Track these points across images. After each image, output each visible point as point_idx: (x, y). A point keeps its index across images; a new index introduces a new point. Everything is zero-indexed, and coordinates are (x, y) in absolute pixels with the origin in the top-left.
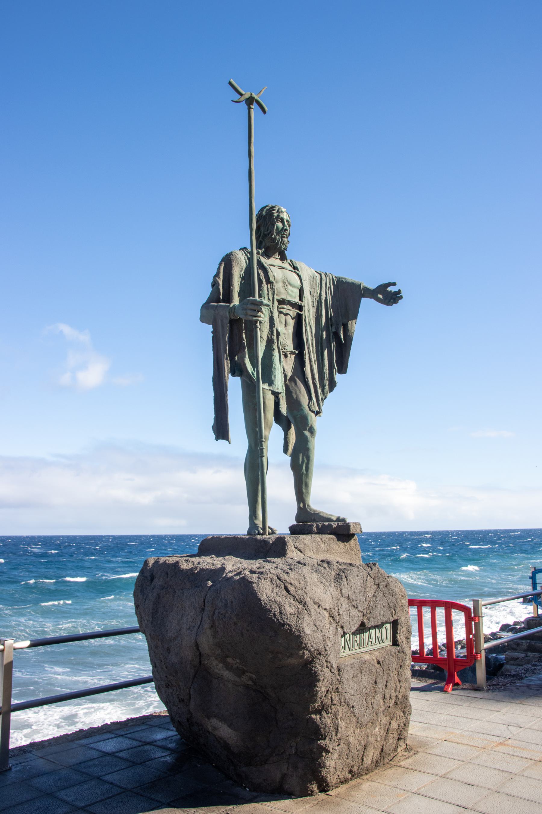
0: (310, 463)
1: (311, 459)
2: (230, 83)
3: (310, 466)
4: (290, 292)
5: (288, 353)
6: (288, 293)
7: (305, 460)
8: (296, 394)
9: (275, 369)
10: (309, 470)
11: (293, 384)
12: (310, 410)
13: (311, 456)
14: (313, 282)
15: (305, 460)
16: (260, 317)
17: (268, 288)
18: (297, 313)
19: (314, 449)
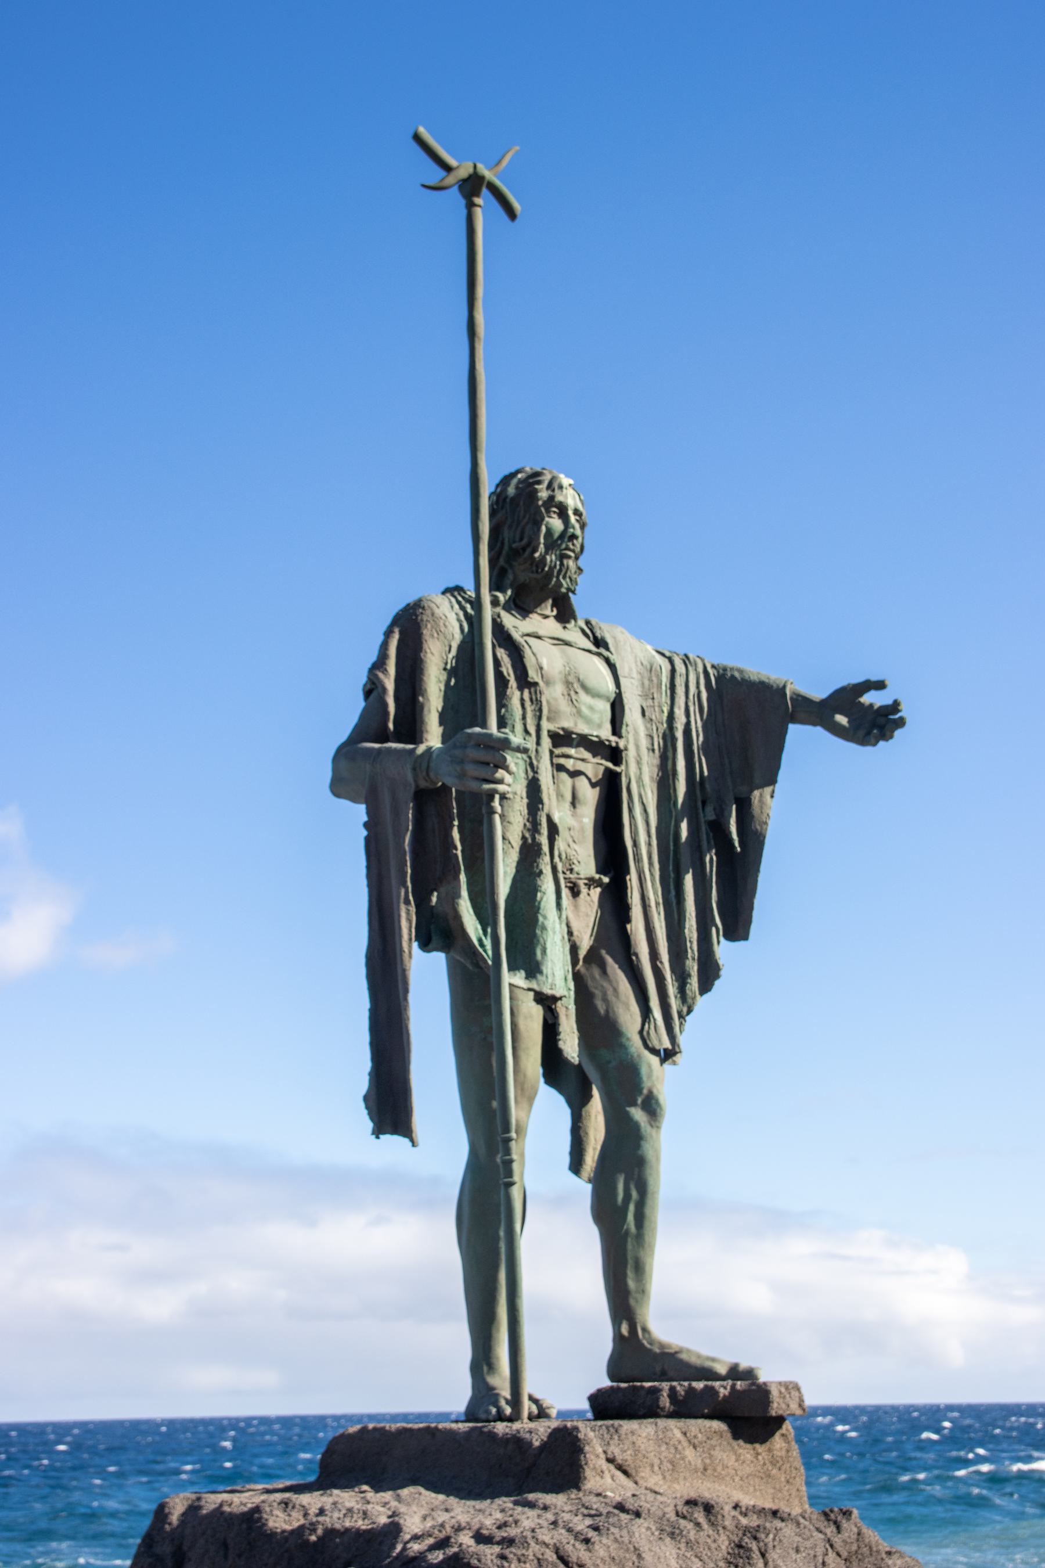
0: (649, 1202)
1: (651, 1188)
2: (417, 138)
3: (647, 1211)
4: (585, 710)
5: (581, 883)
6: (579, 712)
7: (634, 1194)
8: (605, 1000)
9: (544, 928)
10: (647, 1224)
11: (596, 972)
12: (646, 1046)
13: (651, 1181)
14: (651, 680)
15: (634, 1194)
16: (501, 782)
17: (522, 700)
18: (607, 769)
19: (658, 1159)
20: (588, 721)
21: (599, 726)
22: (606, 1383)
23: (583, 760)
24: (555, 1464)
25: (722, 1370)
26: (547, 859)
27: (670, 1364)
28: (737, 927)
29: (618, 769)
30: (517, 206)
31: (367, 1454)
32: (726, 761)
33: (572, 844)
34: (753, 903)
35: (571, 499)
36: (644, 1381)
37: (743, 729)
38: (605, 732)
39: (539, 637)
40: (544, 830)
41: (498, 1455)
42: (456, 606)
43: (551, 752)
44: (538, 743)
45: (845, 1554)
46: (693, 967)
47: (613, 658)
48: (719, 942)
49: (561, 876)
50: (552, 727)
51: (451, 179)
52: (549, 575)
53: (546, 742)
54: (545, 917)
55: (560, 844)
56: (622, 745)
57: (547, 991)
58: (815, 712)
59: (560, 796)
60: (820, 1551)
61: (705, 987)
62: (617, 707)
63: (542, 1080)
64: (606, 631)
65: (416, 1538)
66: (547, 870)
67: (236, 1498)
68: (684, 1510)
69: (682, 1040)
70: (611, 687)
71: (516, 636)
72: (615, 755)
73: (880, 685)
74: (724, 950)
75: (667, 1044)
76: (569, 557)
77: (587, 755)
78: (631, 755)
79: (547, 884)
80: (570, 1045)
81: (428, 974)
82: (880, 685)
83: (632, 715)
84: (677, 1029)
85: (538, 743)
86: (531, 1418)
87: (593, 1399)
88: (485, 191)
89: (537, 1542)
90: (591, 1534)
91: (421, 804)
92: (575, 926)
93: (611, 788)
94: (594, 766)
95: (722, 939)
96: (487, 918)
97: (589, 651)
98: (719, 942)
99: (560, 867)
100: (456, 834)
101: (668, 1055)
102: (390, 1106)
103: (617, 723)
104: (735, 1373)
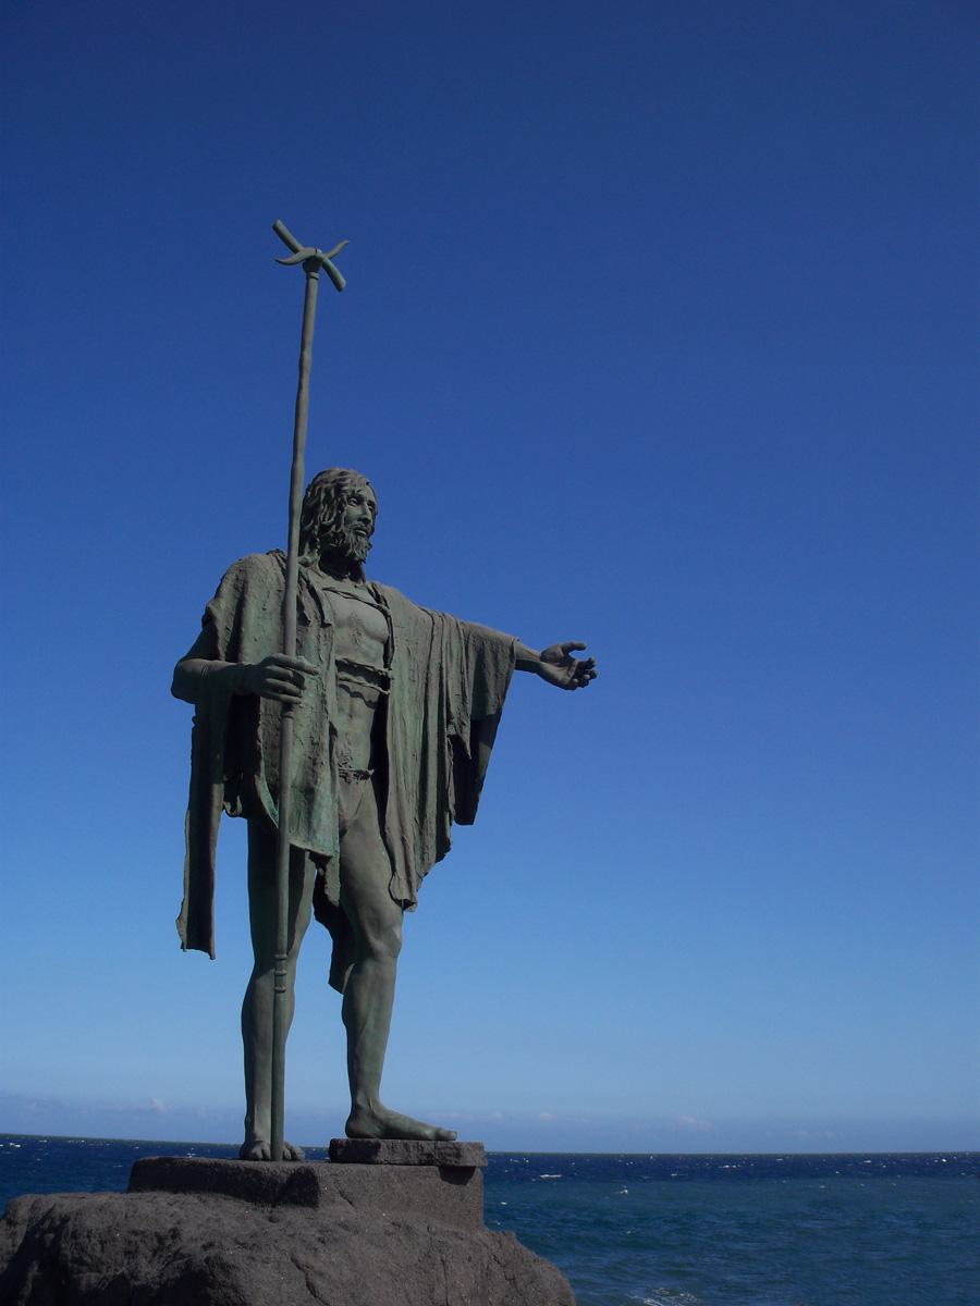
2: (276, 229)
20: (366, 655)
21: (375, 660)
22: (343, 1136)
23: (360, 684)
24: (300, 1189)
25: (428, 1132)
26: (327, 754)
27: (392, 1131)
28: (466, 815)
29: (386, 693)
30: (343, 281)
31: (161, 1169)
32: (323, 648)
33: (348, 746)
34: (476, 800)
35: (367, 494)
36: (367, 1139)
37: (489, 670)
38: (379, 666)
39: (335, 592)
40: (327, 733)
41: (254, 1176)
42: (276, 563)
43: (337, 677)
44: (328, 669)
45: (503, 1262)
46: (431, 842)
47: (390, 612)
48: (451, 824)
49: (337, 768)
50: (339, 658)
51: (295, 258)
52: (347, 547)
53: (333, 667)
54: (322, 797)
55: (340, 745)
56: (390, 674)
57: (318, 850)
58: (526, 665)
59: (341, 709)
60: (485, 1260)
61: (440, 857)
62: (388, 645)
63: (313, 916)
64: (387, 591)
65: (192, 1240)
66: (326, 761)
67: (66, 1203)
68: (391, 1229)
69: (419, 896)
70: (386, 633)
71: (318, 589)
72: (385, 682)
73: (581, 648)
74: (455, 831)
75: (405, 896)
76: (362, 535)
77: (362, 680)
78: (394, 684)
79: (325, 774)
80: (333, 892)
81: (232, 839)
82: (581, 648)
83: (399, 655)
84: (414, 885)
85: (328, 669)
86: (285, 1159)
87: (334, 1143)
88: (321, 268)
89: (277, 1249)
90: (319, 1245)
91: (232, 723)
92: (344, 805)
93: (380, 708)
94: (371, 690)
95: (454, 822)
96: (276, 791)
97: (372, 605)
98: (451, 824)
99: (336, 760)
100: (340, 245)
101: (406, 905)
102: (198, 934)
103: (387, 658)
104: (439, 1137)
